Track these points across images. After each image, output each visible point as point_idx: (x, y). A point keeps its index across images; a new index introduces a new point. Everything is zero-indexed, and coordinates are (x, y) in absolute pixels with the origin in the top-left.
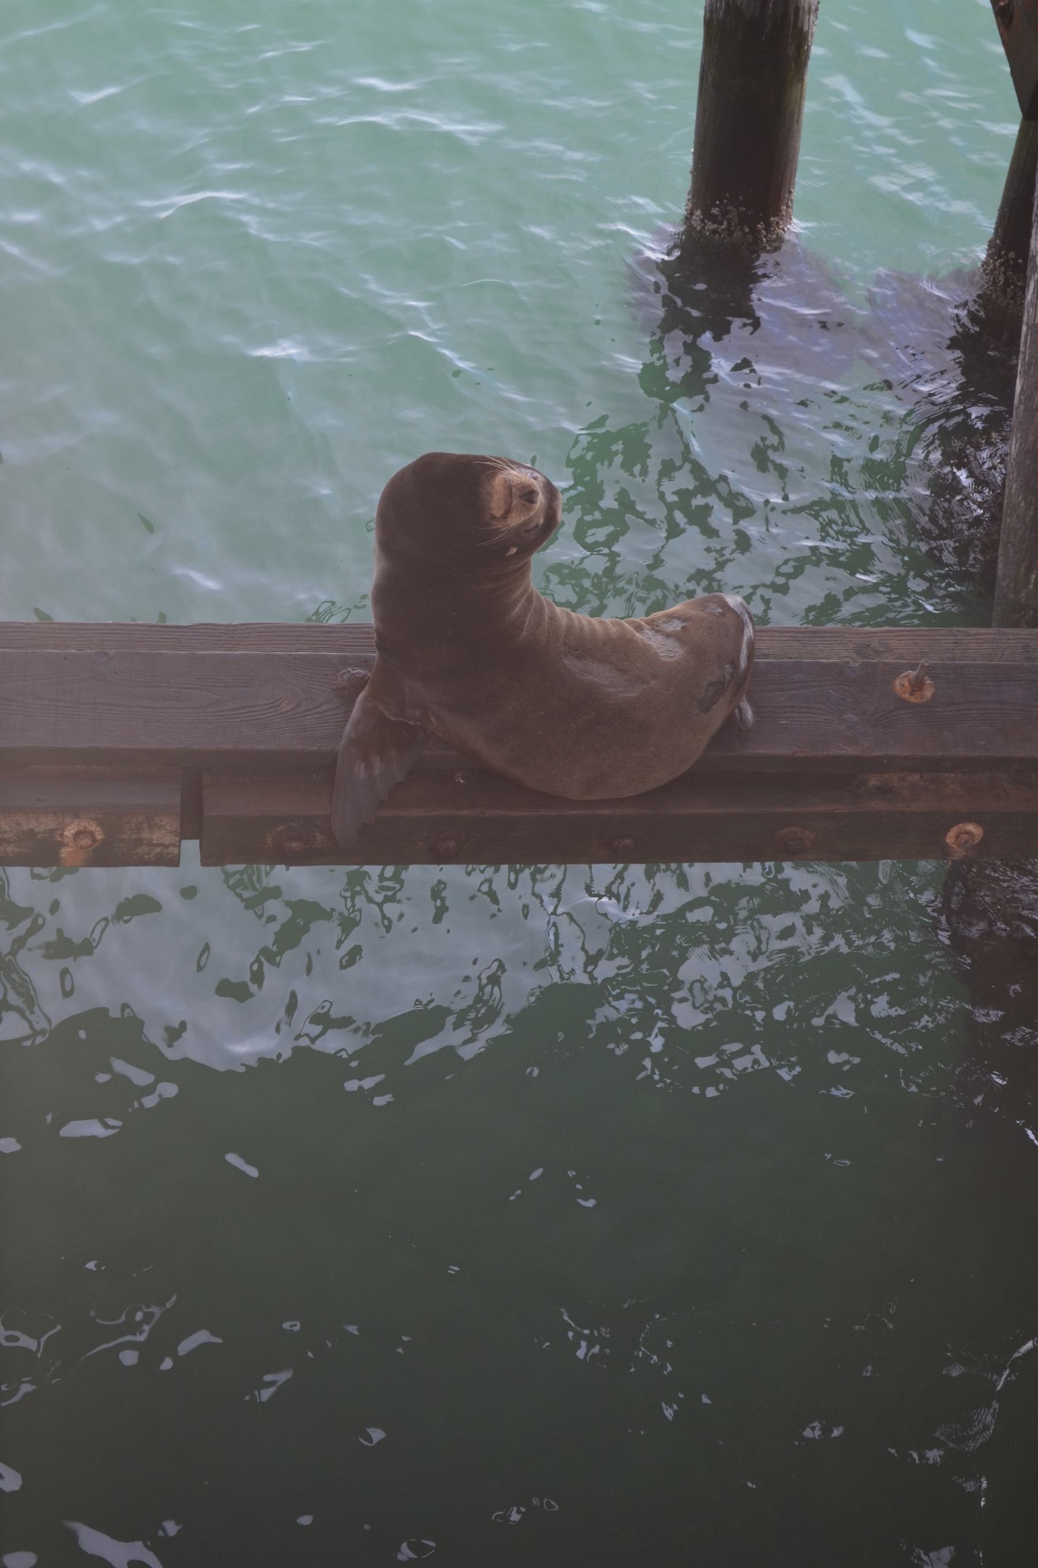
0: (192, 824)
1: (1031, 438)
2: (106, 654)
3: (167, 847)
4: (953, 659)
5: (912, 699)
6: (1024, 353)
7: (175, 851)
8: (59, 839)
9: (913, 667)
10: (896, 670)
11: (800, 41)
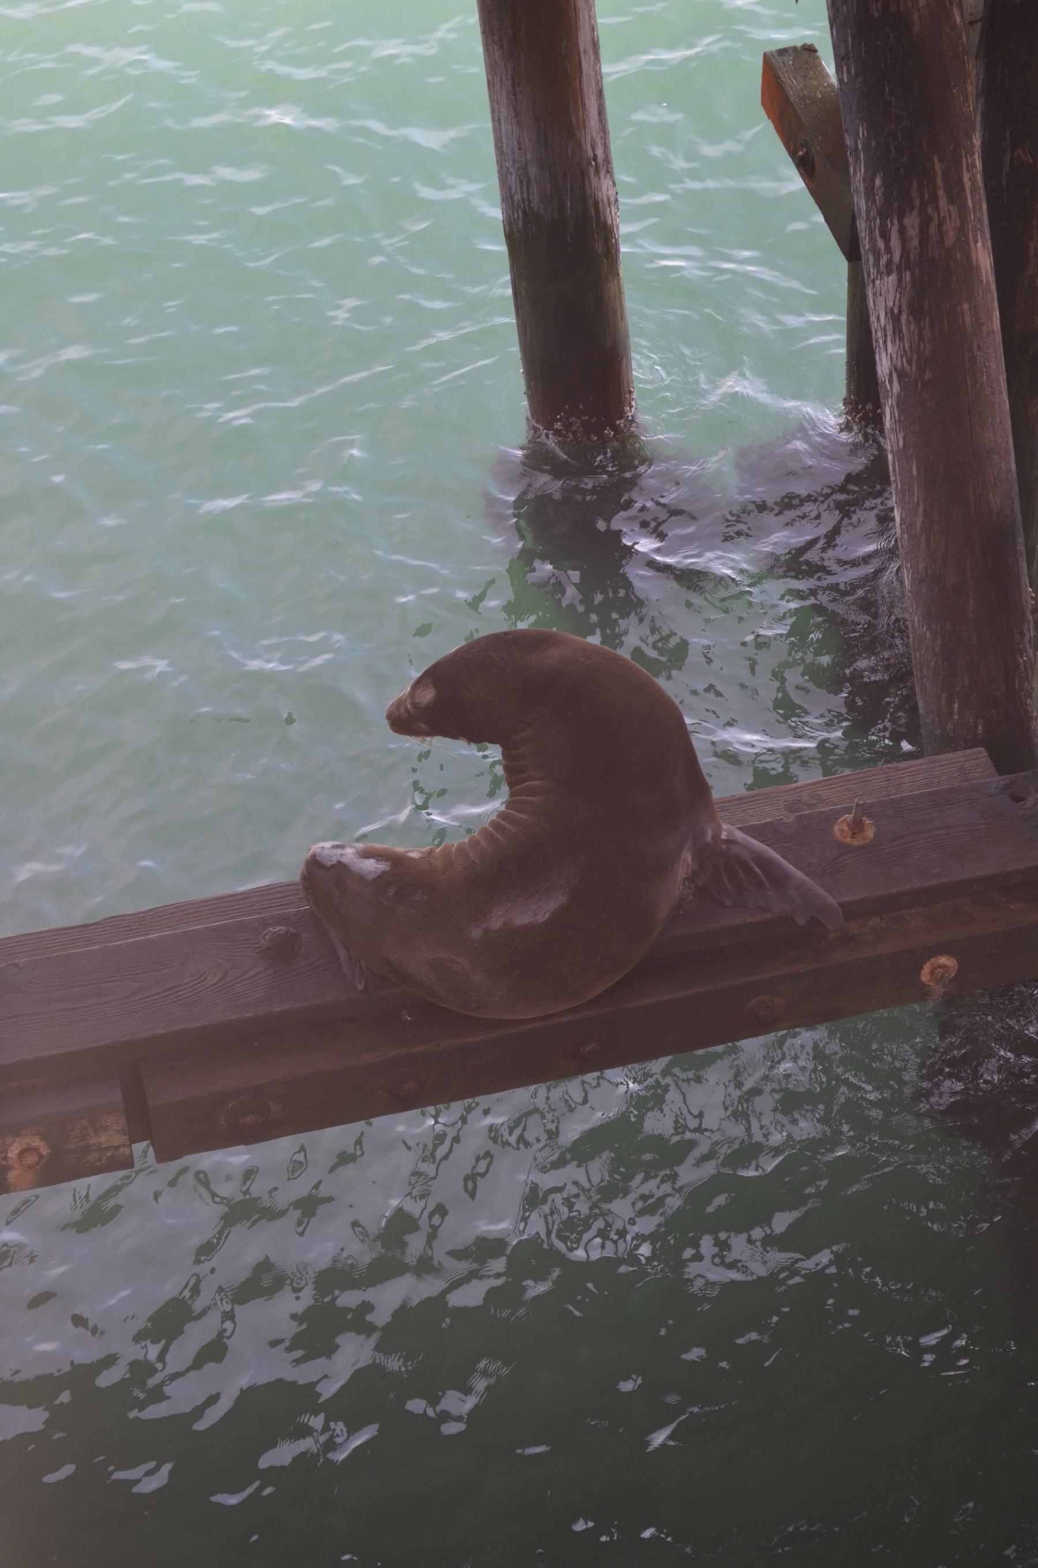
0: (140, 1124)
1: (922, 565)
2: (16, 965)
3: (117, 1148)
4: (889, 795)
5: (855, 843)
6: (895, 481)
7: (127, 1151)
8: (4, 1163)
9: (848, 810)
10: (832, 817)
11: (607, 235)
